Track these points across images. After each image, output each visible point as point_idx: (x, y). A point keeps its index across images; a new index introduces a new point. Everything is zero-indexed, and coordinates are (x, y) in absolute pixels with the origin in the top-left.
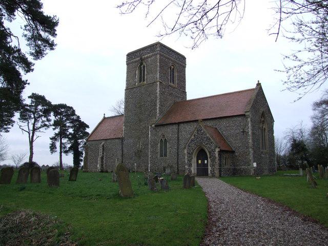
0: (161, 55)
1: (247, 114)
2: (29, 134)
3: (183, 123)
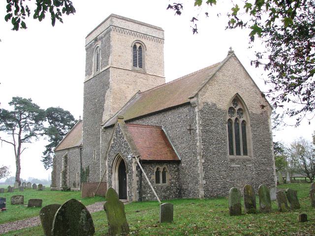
1: (192, 101)
2: (15, 145)
3: (5, 141)
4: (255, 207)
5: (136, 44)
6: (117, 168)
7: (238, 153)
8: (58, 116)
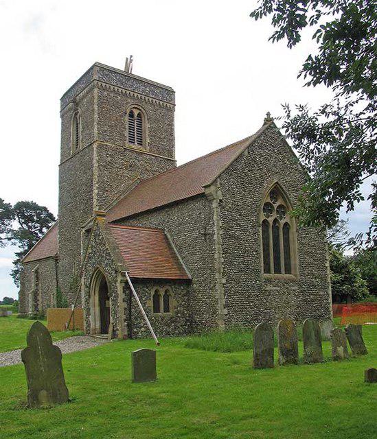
0: (101, 89)
1: (207, 191)
4: (296, 353)
5: (134, 110)
6: (97, 289)
7: (278, 271)
8: (28, 211)
